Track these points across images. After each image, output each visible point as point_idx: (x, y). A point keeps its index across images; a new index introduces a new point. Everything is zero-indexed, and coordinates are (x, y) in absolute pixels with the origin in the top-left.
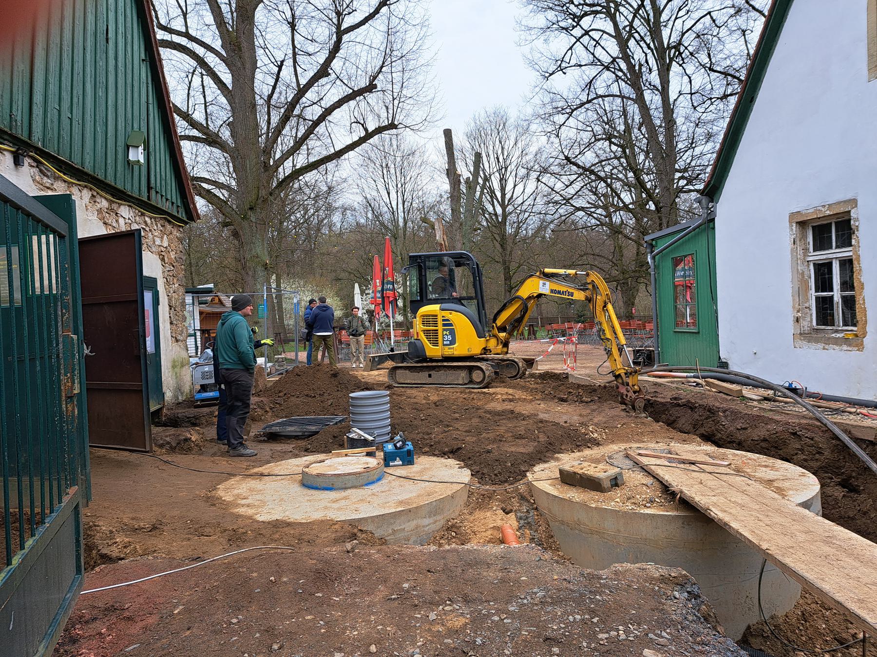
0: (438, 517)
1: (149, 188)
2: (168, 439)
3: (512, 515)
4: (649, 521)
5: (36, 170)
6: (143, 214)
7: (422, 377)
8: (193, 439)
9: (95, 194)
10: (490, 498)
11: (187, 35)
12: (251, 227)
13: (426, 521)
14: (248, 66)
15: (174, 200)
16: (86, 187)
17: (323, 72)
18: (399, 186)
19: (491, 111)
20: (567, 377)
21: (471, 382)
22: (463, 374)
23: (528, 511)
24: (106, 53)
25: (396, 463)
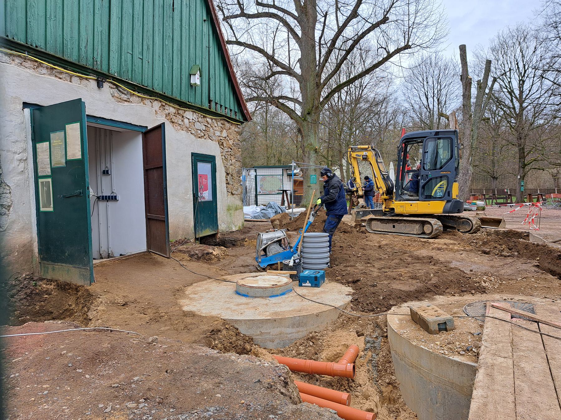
0: (301, 329)
1: (210, 101)
2: (197, 252)
3: (362, 338)
4: (456, 368)
5: (115, 91)
6: (204, 117)
7: (388, 227)
8: (215, 253)
9: (164, 104)
10: (353, 321)
11: (274, 6)
12: (308, 125)
13: (289, 330)
14: (311, 20)
15: (232, 108)
16: (156, 100)
17: (354, 14)
18: (436, 92)
19: (513, 27)
20: (528, 236)
21: (424, 233)
22: (417, 226)
23: (377, 337)
24: (173, 18)
25: (307, 284)
